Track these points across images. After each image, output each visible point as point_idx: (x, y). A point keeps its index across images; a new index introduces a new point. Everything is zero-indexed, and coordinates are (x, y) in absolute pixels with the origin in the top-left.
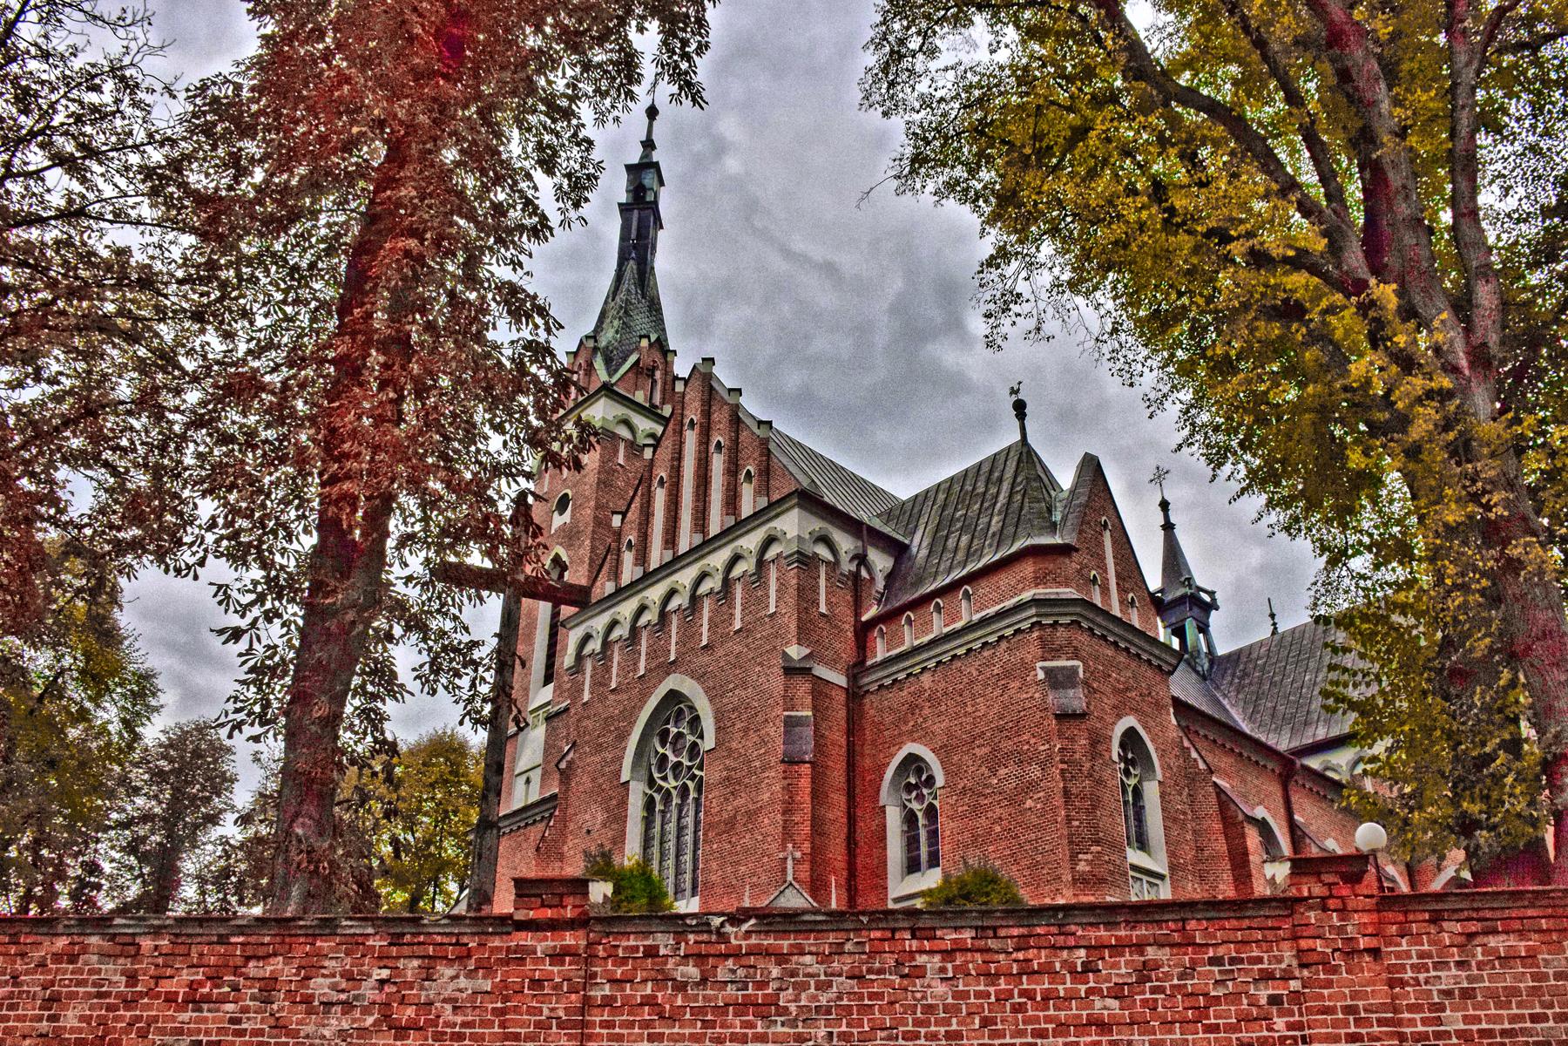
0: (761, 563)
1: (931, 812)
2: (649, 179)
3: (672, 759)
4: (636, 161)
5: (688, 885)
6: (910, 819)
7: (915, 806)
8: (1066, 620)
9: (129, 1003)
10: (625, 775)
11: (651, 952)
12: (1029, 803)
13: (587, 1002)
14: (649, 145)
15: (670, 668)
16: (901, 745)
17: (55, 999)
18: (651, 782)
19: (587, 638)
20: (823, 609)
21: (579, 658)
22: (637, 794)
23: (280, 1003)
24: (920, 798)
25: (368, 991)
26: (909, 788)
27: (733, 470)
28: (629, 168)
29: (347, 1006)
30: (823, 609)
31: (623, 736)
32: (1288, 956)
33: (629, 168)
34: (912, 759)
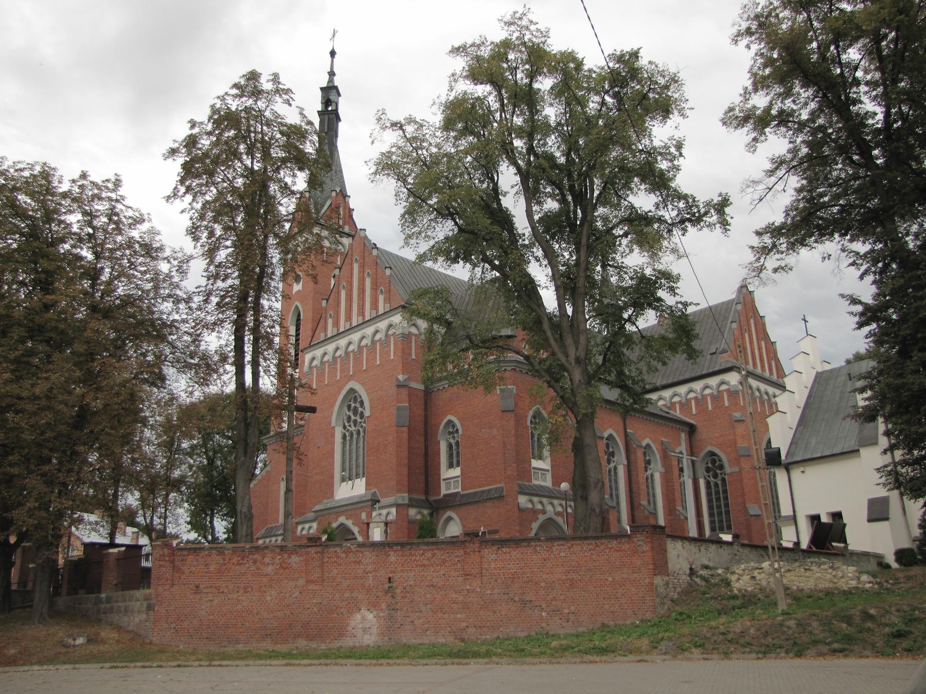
0: (387, 335)
1: (457, 443)
2: (333, 97)
3: (353, 418)
4: (325, 85)
5: (361, 472)
6: (450, 446)
7: (452, 441)
8: (509, 369)
9: (225, 565)
10: (333, 424)
11: (336, 552)
12: (493, 444)
13: (323, 563)
14: (332, 74)
15: (351, 378)
16: (446, 415)
17: (207, 565)
18: (345, 427)
19: (313, 359)
20: (414, 357)
21: (310, 367)
22: (339, 432)
23: (258, 564)
24: (454, 438)
25: (277, 561)
26: (450, 433)
27: (375, 288)
28: (322, 89)
29: (273, 564)
30: (414, 357)
31: (333, 406)
32: (462, 552)
33: (322, 89)
34: (450, 422)
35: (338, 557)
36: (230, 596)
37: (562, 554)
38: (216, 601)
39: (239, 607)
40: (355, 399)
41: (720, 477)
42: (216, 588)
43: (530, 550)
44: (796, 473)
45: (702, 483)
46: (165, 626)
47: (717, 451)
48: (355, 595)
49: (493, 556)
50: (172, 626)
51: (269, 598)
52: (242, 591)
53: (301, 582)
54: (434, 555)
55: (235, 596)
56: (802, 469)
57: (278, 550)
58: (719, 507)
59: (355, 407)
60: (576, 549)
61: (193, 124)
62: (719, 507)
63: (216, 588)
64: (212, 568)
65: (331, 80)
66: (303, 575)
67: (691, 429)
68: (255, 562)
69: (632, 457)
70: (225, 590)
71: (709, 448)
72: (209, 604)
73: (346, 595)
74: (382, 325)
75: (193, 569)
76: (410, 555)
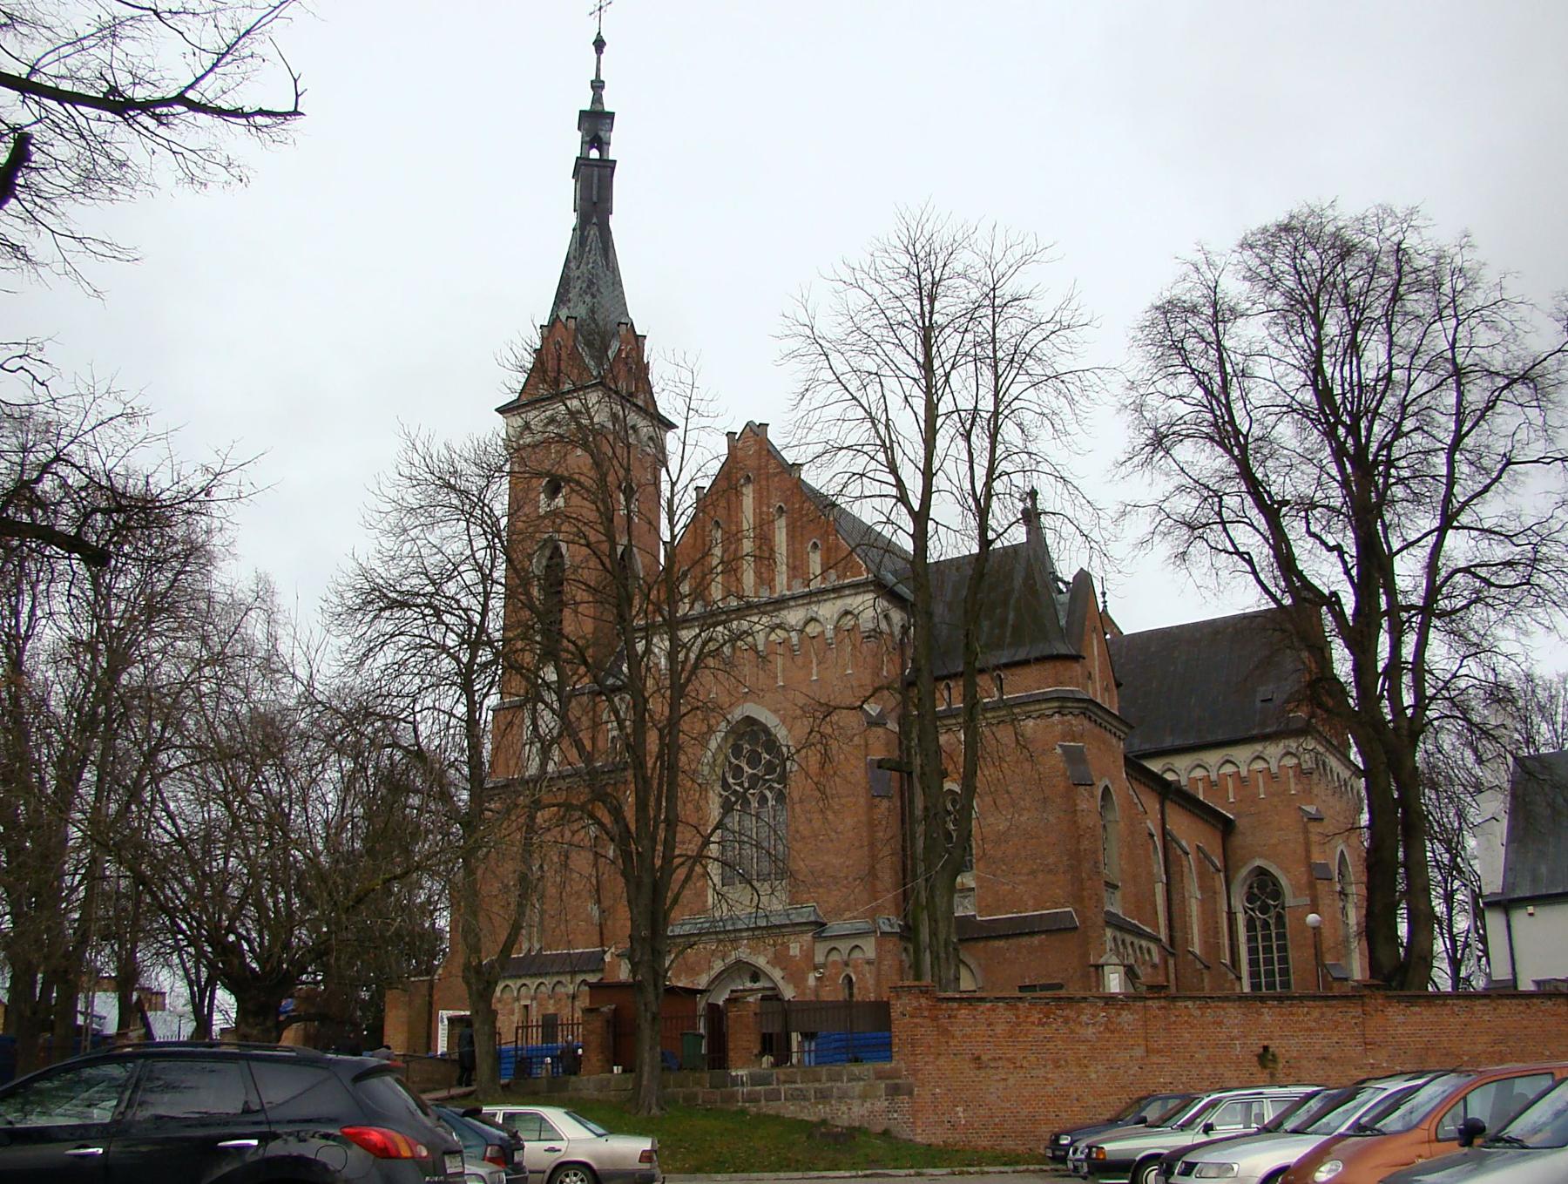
14: (597, 85)
35: (1190, 1015)
36: (1034, 1073)
37: (1487, 1018)
38: (1011, 1081)
39: (1050, 1089)
40: (754, 738)
41: (1273, 913)
42: (1008, 1060)
43: (1446, 1011)
44: (1520, 918)
45: (1241, 919)
46: (933, 1118)
47: (1273, 869)
48: (1220, 1070)
49: (1401, 1018)
50: (945, 1119)
51: (1093, 1076)
52: (1050, 1066)
53: (1139, 1052)
54: (1323, 1014)
55: (1041, 1072)
56: (1531, 909)
57: (1101, 1004)
58: (1269, 962)
59: (753, 751)
60: (1503, 1010)
61: (1132, 385)
62: (1269, 962)
63: (1008, 1060)
64: (999, 1029)
65: (597, 99)
66: (1141, 1041)
67: (1226, 827)
68: (1066, 1022)
69: (1174, 869)
70: (1025, 1064)
71: (1258, 862)
72: (1001, 1085)
73: (1207, 1071)
74: (828, 611)
75: (969, 1031)
76: (1292, 1014)
